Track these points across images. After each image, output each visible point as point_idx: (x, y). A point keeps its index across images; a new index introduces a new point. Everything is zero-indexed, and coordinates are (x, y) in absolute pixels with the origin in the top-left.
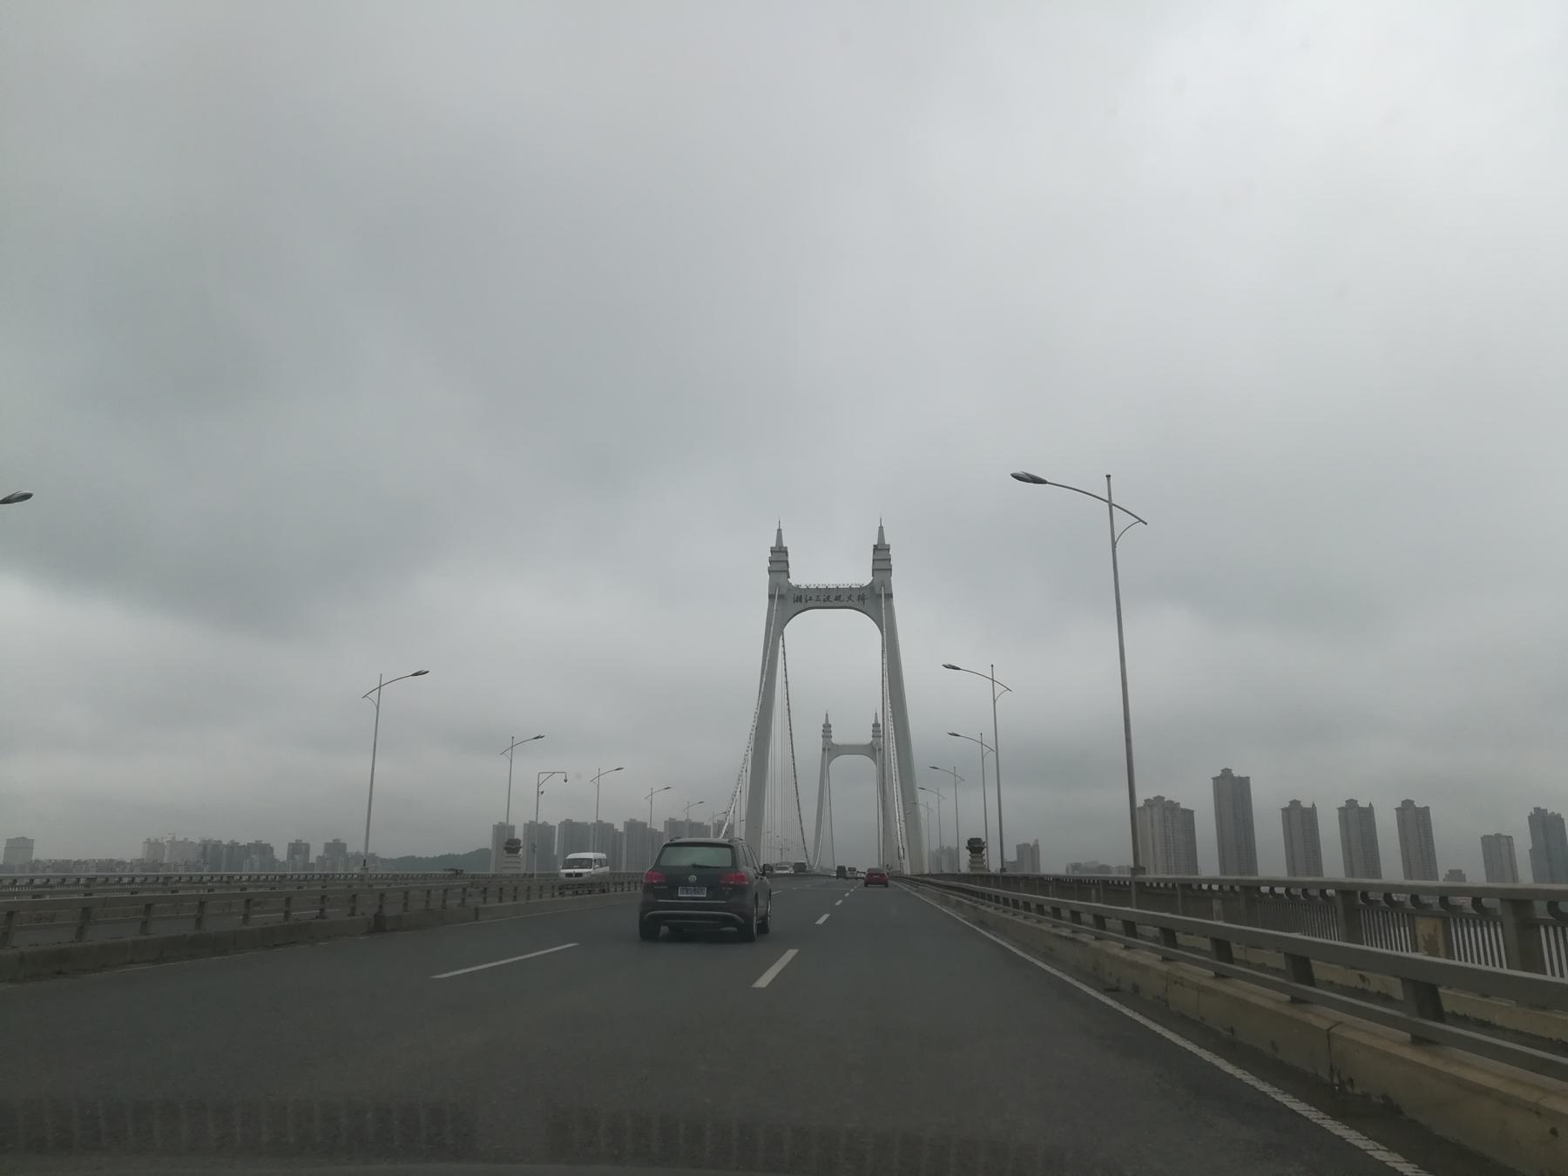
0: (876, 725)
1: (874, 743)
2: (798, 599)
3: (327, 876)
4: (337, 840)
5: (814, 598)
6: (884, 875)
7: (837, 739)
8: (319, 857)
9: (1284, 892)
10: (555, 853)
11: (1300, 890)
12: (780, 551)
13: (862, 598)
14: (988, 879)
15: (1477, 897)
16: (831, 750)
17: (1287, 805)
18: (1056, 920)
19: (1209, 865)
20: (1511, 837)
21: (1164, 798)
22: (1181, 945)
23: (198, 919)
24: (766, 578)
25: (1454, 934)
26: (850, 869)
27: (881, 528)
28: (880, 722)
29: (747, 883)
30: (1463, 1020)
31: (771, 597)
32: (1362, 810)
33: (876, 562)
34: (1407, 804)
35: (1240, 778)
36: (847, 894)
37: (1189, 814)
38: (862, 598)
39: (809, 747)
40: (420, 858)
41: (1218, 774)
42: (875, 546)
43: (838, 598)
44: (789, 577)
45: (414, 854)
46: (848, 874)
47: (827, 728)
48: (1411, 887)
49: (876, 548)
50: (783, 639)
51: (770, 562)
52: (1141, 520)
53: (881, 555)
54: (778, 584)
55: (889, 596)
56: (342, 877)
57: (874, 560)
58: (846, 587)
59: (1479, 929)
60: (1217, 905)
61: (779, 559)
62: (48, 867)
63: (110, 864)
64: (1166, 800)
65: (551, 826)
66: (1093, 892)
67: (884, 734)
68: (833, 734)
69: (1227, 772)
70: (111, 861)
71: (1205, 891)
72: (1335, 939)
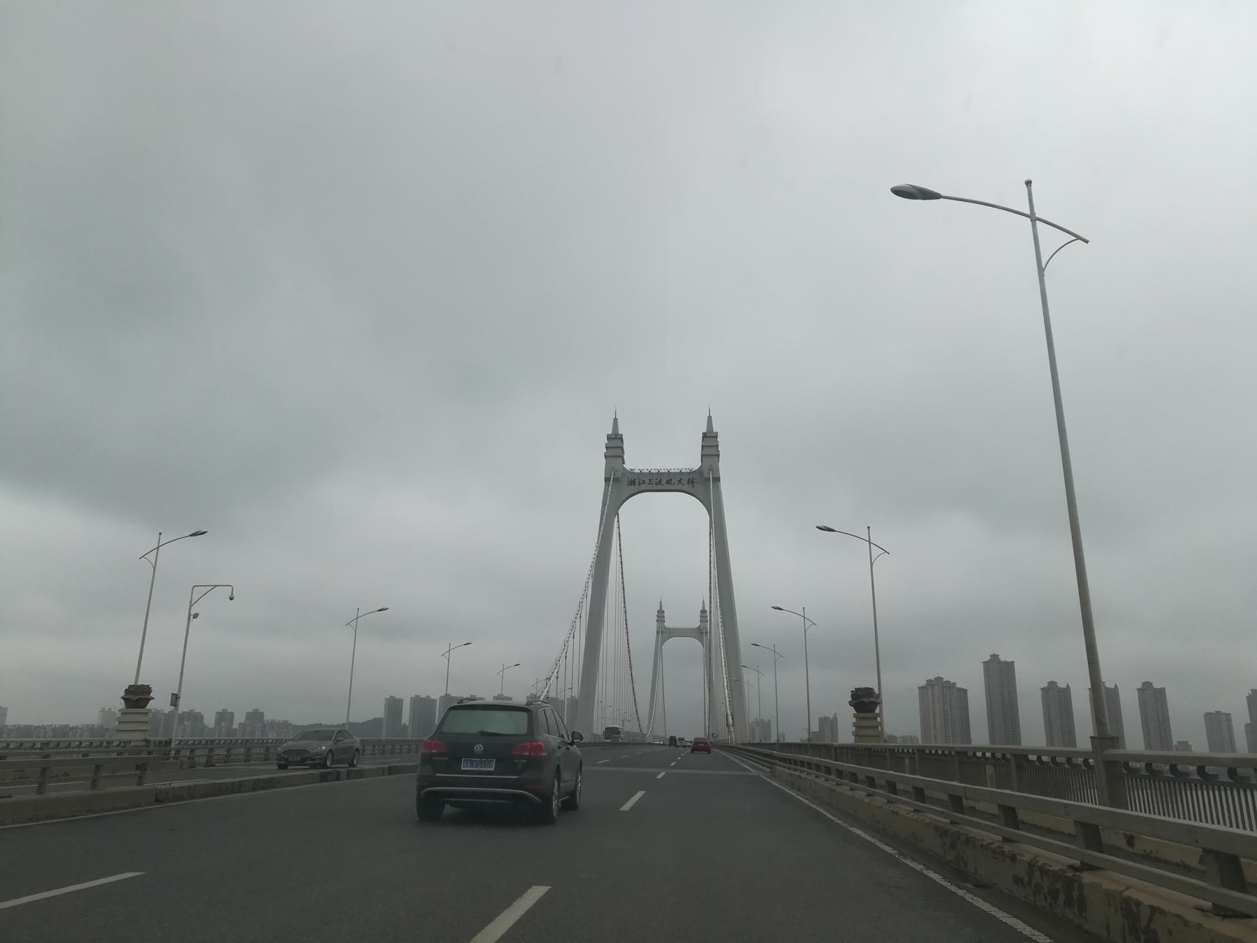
0: (703, 611)
1: (702, 627)
2: (632, 483)
3: (247, 741)
5: (647, 481)
7: (669, 623)
8: (240, 724)
9: (1036, 759)
11: (1143, 764)
12: (616, 438)
13: (691, 482)
14: (896, 755)
16: (664, 633)
17: (1046, 685)
18: (853, 784)
19: (980, 736)
20: (1229, 714)
21: (943, 678)
22: (1022, 822)
23: (93, 780)
24: (602, 462)
26: (679, 739)
27: (710, 418)
28: (707, 608)
29: (545, 754)
30: (1035, 828)
31: (607, 480)
33: (704, 449)
34: (1147, 685)
35: (1006, 663)
36: (679, 758)
37: (964, 692)
38: (691, 482)
39: (644, 634)
41: (988, 658)
42: (703, 433)
43: (669, 482)
44: (624, 463)
45: (322, 722)
46: (678, 743)
48: (992, 748)
49: (704, 435)
52: (1079, 238)
53: (710, 442)
54: (613, 468)
55: (717, 480)
57: (702, 446)
58: (676, 471)
60: (989, 770)
61: (615, 445)
62: (13, 730)
63: (65, 730)
64: (944, 680)
66: (907, 761)
67: (710, 619)
68: (665, 619)
69: (995, 657)
70: (66, 726)
71: (979, 757)
72: (1169, 816)
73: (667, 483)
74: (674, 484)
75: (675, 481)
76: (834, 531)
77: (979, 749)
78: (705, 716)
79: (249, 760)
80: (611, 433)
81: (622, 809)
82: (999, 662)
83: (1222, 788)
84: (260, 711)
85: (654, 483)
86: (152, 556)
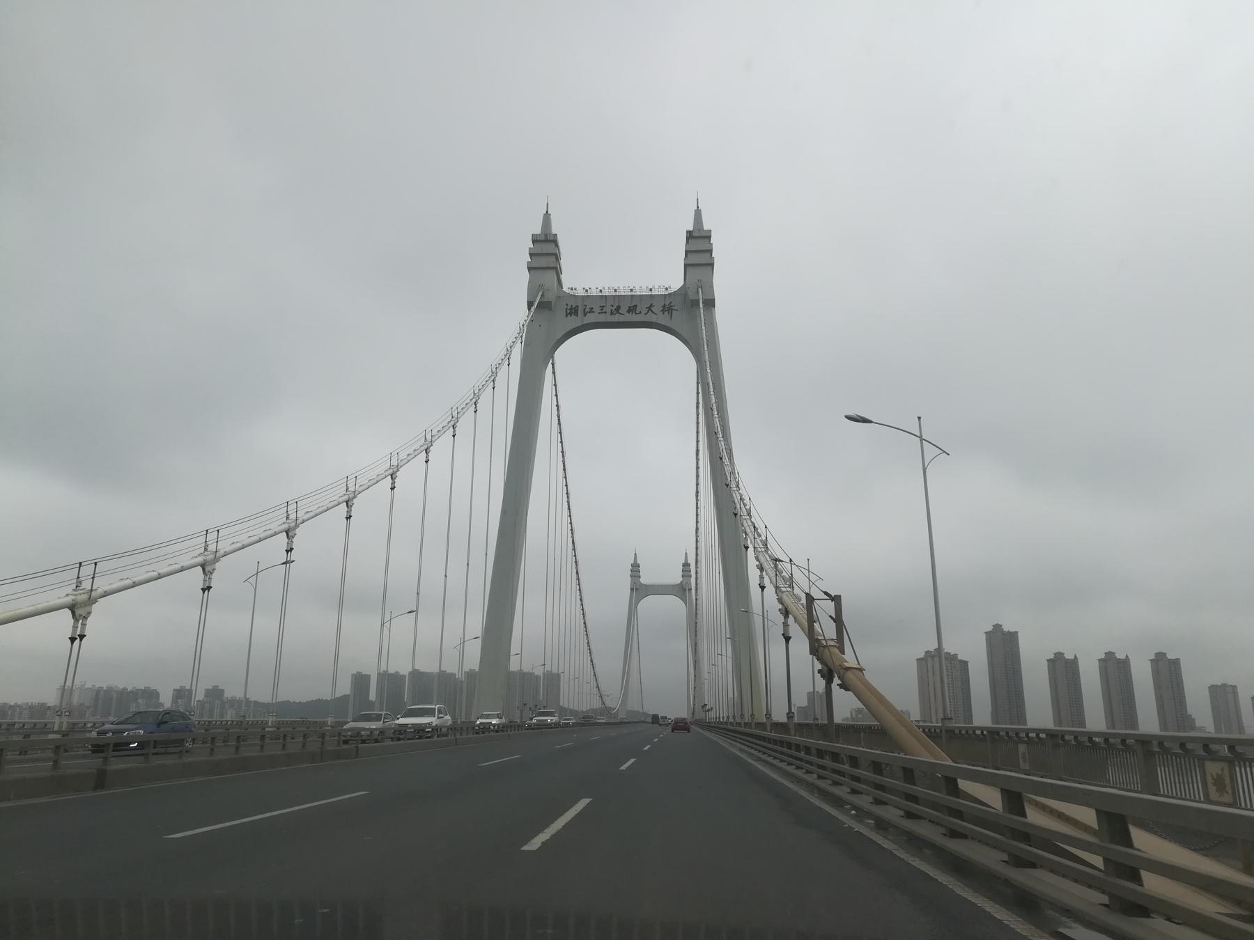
2: (573, 311)
4: (216, 686)
5: (597, 309)
6: (687, 723)
7: (645, 579)
10: (405, 700)
11: (1119, 740)
13: (668, 309)
15: (1206, 744)
16: (639, 590)
20: (1235, 686)
25: (1238, 774)
26: (662, 718)
28: (692, 561)
32: (1119, 661)
33: (690, 270)
37: (965, 664)
40: (294, 702)
41: (990, 628)
42: (688, 232)
43: (632, 309)
46: (661, 722)
47: (635, 568)
49: (690, 236)
50: (553, 364)
51: (531, 255)
54: (541, 286)
55: (710, 303)
56: (229, 723)
57: (686, 266)
59: (1163, 768)
65: (365, 675)
68: (641, 569)
69: (997, 627)
73: (628, 312)
74: (640, 313)
75: (642, 307)
76: (870, 422)
77: (979, 728)
78: (688, 693)
79: (228, 741)
80: (539, 232)
81: (525, 848)
82: (1003, 633)
83: (1247, 763)
84: (220, 688)
85: (609, 312)
86: (253, 580)
